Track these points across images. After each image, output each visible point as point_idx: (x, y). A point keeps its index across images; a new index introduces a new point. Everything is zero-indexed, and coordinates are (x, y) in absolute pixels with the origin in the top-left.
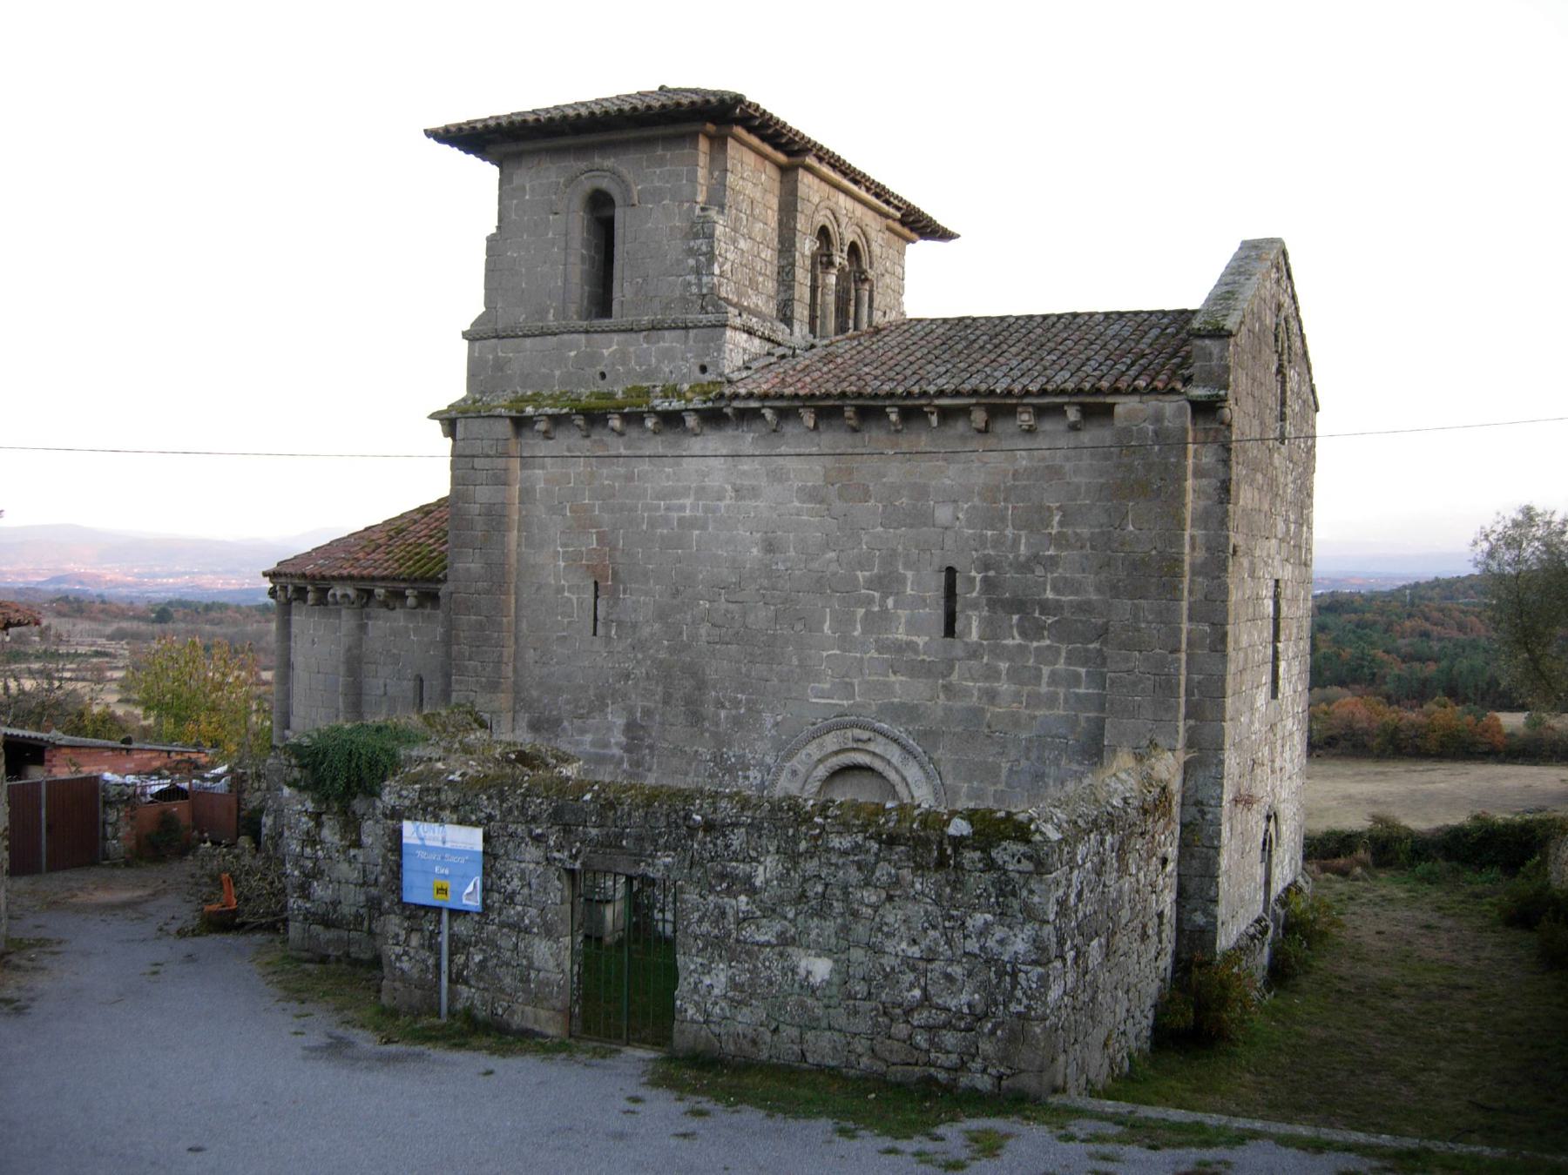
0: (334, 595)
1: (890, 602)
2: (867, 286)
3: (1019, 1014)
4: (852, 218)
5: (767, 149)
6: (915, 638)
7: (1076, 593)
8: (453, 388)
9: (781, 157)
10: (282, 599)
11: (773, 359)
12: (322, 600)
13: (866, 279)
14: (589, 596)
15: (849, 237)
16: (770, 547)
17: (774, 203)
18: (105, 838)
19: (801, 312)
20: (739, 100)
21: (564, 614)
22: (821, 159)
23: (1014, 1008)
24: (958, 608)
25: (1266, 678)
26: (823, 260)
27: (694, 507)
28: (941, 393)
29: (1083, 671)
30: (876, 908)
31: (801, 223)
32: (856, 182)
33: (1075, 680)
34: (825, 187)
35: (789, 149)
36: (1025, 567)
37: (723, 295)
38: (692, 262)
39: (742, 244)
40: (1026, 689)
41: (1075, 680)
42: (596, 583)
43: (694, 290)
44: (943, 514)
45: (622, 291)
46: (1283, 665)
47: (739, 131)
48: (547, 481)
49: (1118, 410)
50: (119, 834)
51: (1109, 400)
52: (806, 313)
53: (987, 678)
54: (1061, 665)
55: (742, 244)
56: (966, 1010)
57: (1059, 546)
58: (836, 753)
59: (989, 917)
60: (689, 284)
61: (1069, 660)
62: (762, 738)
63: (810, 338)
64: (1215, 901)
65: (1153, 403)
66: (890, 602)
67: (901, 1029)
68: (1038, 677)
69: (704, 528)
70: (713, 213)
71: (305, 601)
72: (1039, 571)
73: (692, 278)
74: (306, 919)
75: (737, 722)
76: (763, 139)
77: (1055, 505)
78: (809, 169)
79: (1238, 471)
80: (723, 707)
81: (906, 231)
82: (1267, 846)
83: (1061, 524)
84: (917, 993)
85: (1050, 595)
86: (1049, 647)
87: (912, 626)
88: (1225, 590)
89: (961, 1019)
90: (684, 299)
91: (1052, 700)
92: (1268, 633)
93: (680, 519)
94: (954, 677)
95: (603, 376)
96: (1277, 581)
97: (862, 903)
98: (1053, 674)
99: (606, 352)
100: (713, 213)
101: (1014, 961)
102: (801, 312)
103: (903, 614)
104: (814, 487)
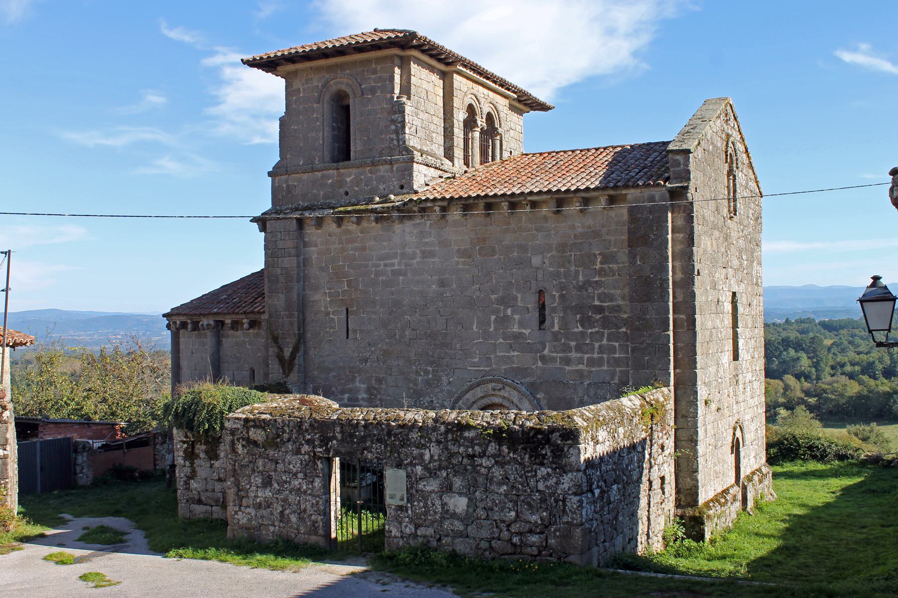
0: (203, 325)
1: (509, 312)
2: (498, 137)
3: (568, 523)
4: (489, 101)
5: (433, 62)
6: (524, 331)
7: (612, 301)
8: (265, 204)
9: (442, 67)
10: (174, 329)
11: (443, 180)
12: (196, 327)
13: (498, 134)
14: (344, 316)
15: (487, 108)
16: (442, 284)
17: (440, 92)
18: (75, 473)
19: (459, 153)
20: (413, 35)
21: (331, 328)
22: (465, 66)
23: (565, 519)
24: (547, 313)
25: (729, 346)
26: (470, 124)
27: (400, 264)
28: (531, 193)
29: (617, 344)
30: (489, 469)
31: (457, 103)
32: (488, 79)
33: (612, 350)
34: (470, 83)
35: (443, 61)
36: (582, 288)
37: (411, 144)
38: (393, 127)
39: (421, 115)
40: (586, 356)
41: (612, 350)
42: (347, 309)
43: (395, 142)
44: (536, 261)
45: (356, 146)
46: (741, 343)
47: (415, 53)
48: (318, 254)
49: (629, 197)
50: (85, 476)
51: (624, 192)
52: (462, 153)
53: (564, 351)
54: (605, 342)
55: (421, 115)
56: (539, 522)
57: (600, 275)
58: (482, 398)
59: (549, 470)
60: (392, 140)
61: (609, 340)
62: (441, 391)
63: (465, 168)
64: (696, 471)
65: (647, 192)
66: (509, 312)
67: (505, 534)
68: (593, 349)
69: (405, 275)
70: (404, 99)
71: (187, 329)
72: (590, 290)
73: (394, 136)
74: (187, 501)
75: (428, 383)
76: (431, 56)
77: (597, 253)
78: (460, 73)
79: (698, 229)
80: (420, 375)
81: (521, 106)
82: (736, 447)
83: (601, 263)
84: (513, 514)
85: (597, 303)
86: (597, 332)
87: (521, 324)
88: (693, 295)
89: (537, 527)
90: (391, 149)
91: (600, 362)
92: (728, 321)
93: (392, 271)
94: (546, 352)
95: (347, 193)
96: (734, 294)
97: (481, 465)
98: (600, 347)
99: (348, 180)
100: (404, 99)
101: (565, 493)
102: (459, 153)
103: (517, 317)
104: (465, 249)
